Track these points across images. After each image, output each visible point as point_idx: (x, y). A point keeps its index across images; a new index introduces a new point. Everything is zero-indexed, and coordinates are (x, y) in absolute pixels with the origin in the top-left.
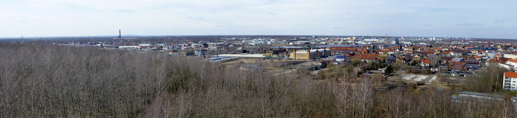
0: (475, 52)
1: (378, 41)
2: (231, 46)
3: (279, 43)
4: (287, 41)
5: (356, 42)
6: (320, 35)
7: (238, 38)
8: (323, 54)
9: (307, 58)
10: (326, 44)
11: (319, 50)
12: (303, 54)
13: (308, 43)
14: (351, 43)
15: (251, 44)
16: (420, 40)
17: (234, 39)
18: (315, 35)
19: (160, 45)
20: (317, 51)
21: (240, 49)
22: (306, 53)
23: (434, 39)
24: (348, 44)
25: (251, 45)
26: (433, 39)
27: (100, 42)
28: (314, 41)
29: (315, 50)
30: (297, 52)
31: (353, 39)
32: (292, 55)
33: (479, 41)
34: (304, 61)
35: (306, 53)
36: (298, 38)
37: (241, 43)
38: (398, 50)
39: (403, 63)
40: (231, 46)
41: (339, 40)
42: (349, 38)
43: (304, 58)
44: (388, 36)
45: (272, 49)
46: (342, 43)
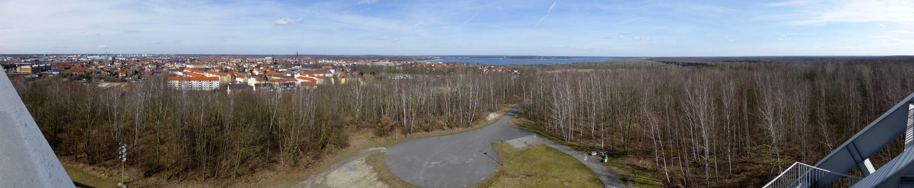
6: (52, 53)
8: (44, 69)
9: (30, 71)
12: (27, 69)
13: (38, 60)
16: (135, 56)
17: (469, 58)
18: (46, 53)
27: (315, 75)
30: (22, 67)
32: (18, 70)
34: (27, 74)
36: (31, 56)
41: (65, 58)
44: (108, 53)
46: (67, 60)
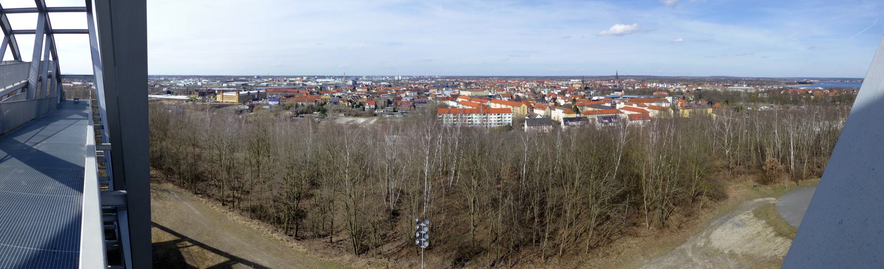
0: (434, 90)
1: (332, 81)
2: (157, 86)
3: (211, 85)
4: (220, 82)
5: (305, 83)
6: (265, 74)
7: (167, 78)
8: (256, 97)
9: (235, 100)
10: (267, 85)
11: (251, 92)
12: (231, 97)
13: (246, 84)
14: (299, 84)
15: (180, 85)
16: (384, 79)
17: (163, 79)
19: (90, 83)
20: (249, 93)
21: (165, 89)
22: (235, 95)
23: (400, 78)
24: (295, 84)
25: (178, 86)
26: (399, 79)
28: (254, 82)
29: (246, 92)
31: (304, 79)
32: (219, 98)
33: (447, 78)
34: (232, 104)
35: (235, 95)
36: (236, 79)
37: (168, 83)
38: (349, 91)
39: (347, 105)
40: (157, 86)
41: (285, 81)
42: (299, 78)
43: (233, 101)
44: (346, 75)
45: (198, 91)
46: (287, 84)
